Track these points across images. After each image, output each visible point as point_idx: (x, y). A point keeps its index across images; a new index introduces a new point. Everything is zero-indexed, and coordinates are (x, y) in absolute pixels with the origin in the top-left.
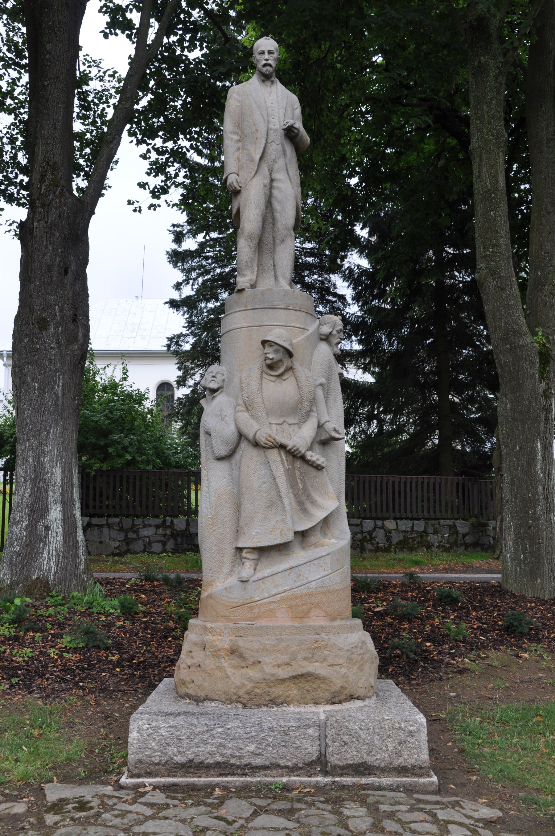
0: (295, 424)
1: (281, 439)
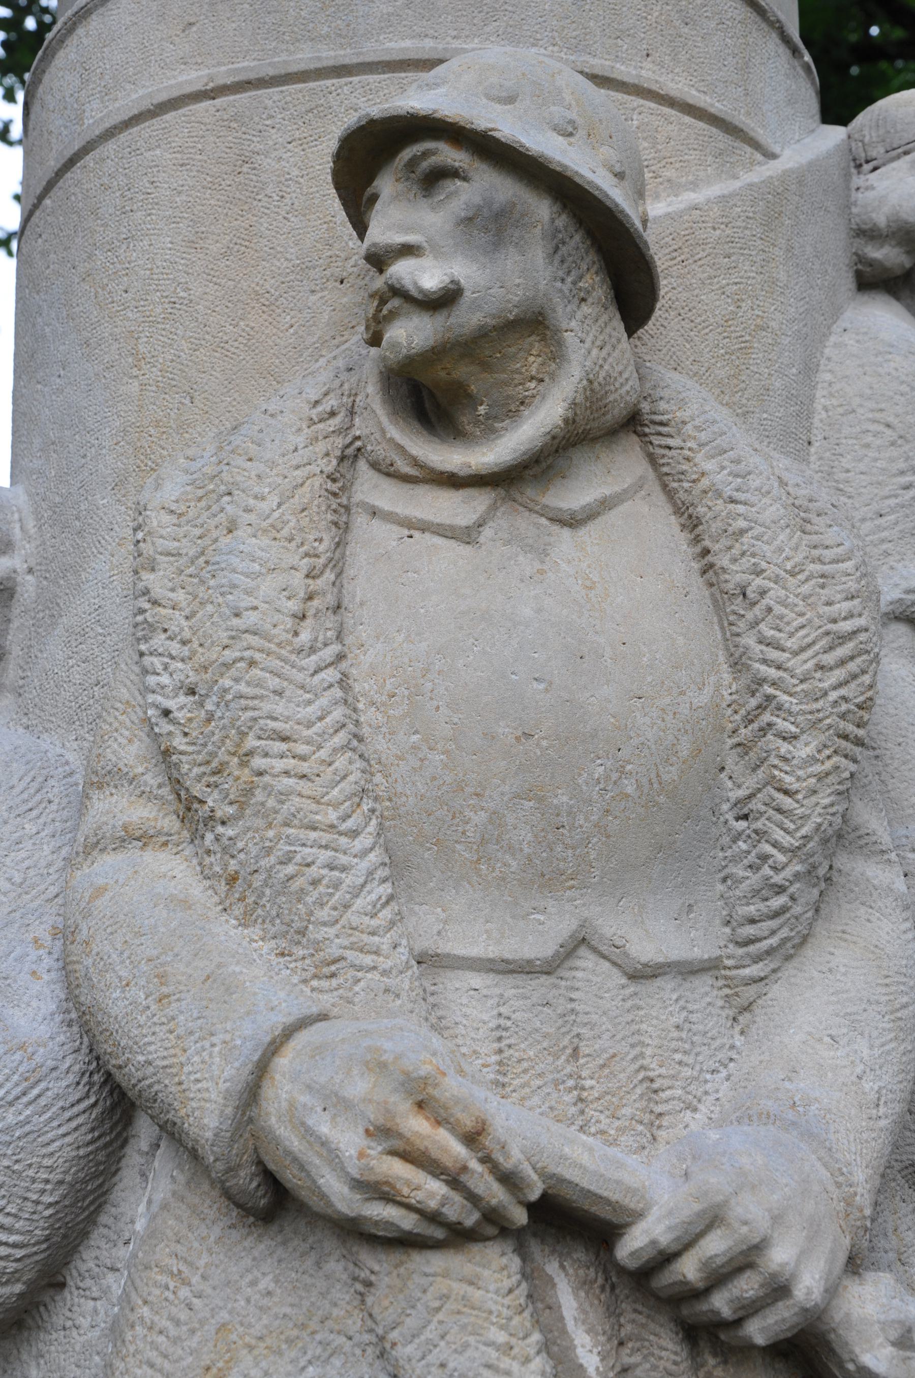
0: (689, 970)
1: (554, 1138)
